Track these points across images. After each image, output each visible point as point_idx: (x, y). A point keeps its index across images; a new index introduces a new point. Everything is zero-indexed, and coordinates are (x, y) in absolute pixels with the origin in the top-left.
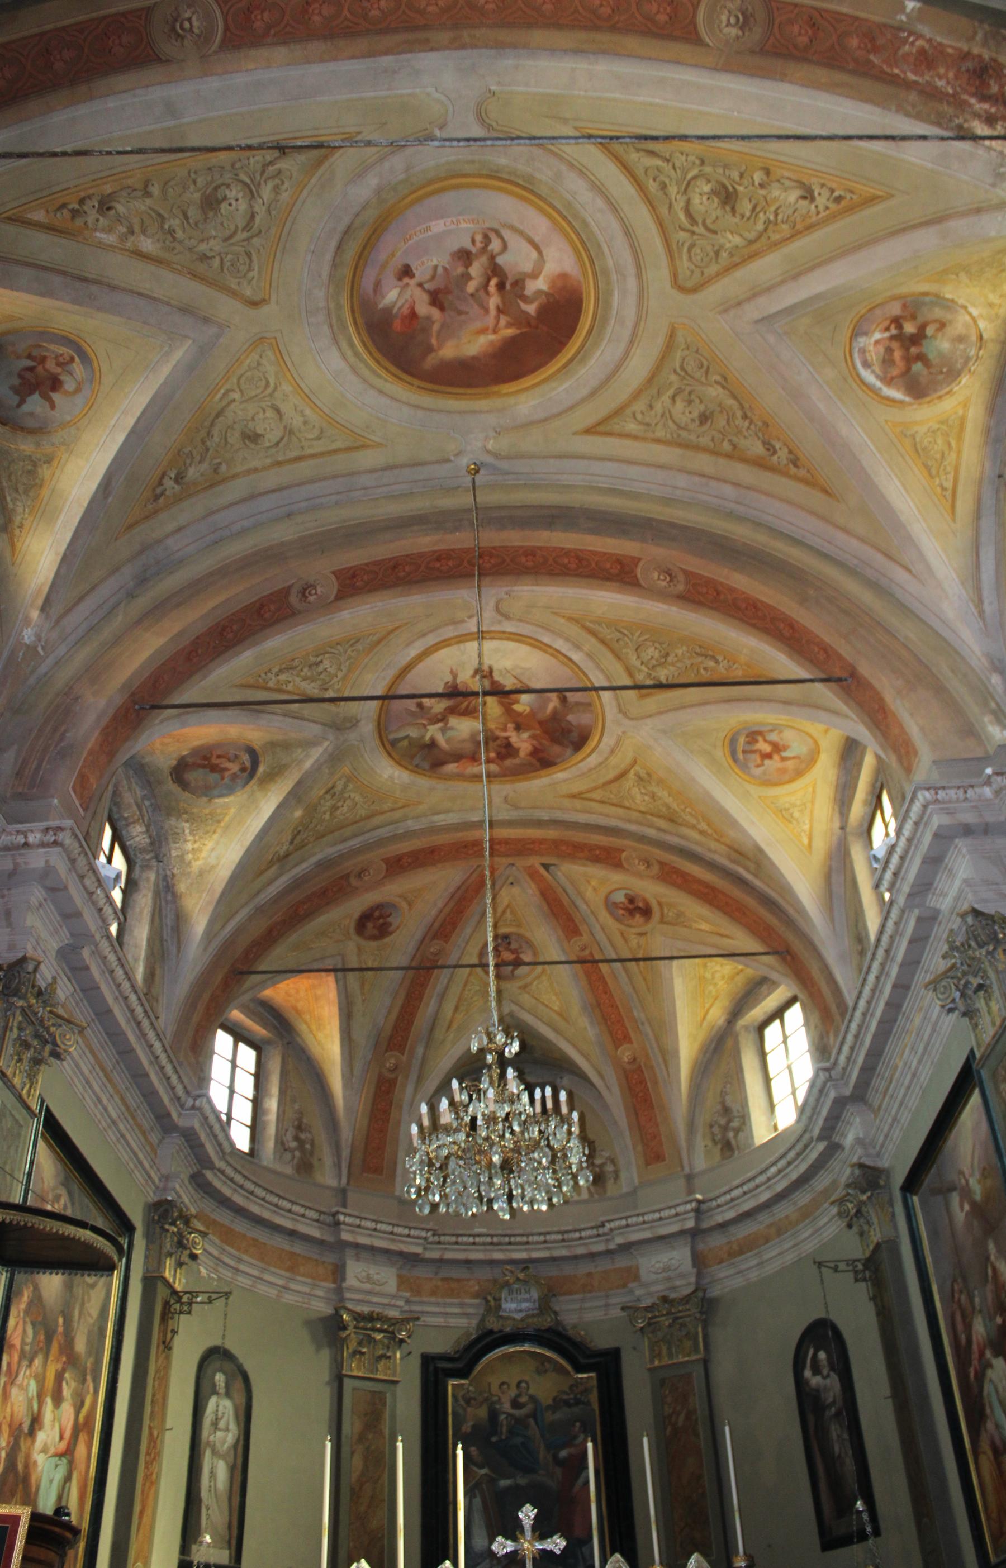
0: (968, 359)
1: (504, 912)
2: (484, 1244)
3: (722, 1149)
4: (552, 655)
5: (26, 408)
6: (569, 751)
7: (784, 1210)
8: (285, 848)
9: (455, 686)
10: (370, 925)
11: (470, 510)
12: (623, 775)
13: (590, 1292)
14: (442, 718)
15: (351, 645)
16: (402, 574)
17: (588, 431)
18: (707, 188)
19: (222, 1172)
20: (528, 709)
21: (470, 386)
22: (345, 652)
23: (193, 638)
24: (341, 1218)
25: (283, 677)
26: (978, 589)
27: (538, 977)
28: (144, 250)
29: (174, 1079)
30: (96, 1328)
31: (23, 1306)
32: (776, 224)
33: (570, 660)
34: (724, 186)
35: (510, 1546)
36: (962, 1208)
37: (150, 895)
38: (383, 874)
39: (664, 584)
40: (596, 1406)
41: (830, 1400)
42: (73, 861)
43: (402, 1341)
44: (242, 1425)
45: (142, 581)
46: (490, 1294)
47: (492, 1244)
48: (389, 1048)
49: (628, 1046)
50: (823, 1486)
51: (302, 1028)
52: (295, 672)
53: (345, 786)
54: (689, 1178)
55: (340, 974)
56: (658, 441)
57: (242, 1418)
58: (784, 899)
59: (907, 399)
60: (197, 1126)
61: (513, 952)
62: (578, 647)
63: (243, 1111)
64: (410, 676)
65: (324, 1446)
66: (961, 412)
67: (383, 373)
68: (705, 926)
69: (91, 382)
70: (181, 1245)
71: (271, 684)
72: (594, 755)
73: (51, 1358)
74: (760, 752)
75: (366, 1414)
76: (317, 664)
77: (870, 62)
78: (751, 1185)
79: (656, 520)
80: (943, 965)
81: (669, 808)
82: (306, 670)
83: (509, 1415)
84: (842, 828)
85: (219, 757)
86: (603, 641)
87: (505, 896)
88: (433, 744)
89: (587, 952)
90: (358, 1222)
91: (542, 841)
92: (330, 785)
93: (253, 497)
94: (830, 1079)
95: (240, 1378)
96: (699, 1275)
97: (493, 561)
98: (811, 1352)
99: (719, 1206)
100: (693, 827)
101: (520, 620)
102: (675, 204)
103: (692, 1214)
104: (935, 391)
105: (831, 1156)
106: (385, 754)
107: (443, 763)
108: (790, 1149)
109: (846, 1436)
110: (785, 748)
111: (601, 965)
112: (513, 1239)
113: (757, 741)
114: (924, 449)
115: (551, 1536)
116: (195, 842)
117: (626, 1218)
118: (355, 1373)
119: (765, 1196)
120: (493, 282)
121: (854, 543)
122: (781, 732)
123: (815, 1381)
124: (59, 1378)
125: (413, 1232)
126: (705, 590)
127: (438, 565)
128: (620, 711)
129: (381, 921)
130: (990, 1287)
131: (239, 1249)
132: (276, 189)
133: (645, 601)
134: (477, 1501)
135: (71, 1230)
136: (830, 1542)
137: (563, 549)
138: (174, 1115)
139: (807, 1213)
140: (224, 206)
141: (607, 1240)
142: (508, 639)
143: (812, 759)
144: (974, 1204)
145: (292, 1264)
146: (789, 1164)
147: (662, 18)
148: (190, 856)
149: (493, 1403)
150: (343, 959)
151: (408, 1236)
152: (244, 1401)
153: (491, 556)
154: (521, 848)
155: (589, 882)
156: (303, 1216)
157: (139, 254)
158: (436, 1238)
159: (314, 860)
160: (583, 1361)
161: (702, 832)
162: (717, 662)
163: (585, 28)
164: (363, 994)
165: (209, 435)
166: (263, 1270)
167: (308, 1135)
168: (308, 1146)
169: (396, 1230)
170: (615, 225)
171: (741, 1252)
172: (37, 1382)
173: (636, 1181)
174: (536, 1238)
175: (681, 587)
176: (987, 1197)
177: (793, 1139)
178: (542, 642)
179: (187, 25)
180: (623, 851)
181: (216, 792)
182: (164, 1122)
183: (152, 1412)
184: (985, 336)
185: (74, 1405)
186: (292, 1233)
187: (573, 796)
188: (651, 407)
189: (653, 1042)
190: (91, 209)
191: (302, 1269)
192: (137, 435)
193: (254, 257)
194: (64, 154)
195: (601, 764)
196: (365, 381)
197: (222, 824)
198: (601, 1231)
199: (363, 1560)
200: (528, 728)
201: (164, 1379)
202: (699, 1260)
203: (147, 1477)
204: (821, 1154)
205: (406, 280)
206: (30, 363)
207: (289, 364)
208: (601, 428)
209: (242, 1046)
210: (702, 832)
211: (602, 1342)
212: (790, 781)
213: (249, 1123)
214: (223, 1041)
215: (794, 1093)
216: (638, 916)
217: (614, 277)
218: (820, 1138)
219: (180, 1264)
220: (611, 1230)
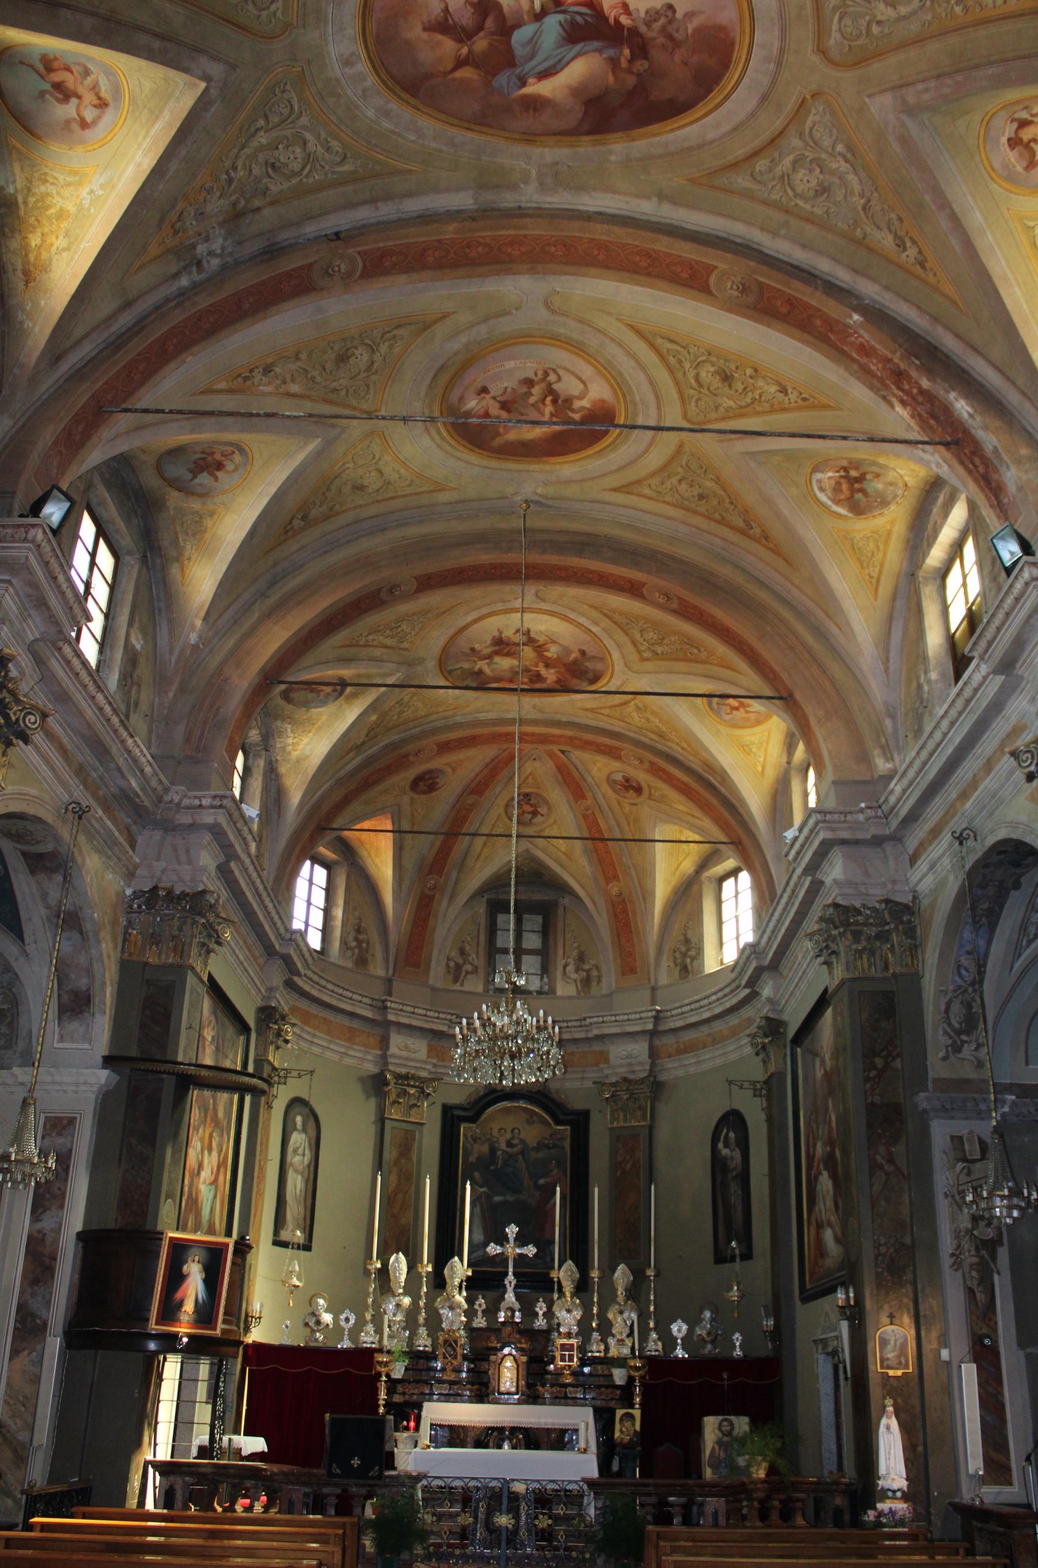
0: (895, 496)
1: (527, 778)
5: (197, 481)
7: (718, 1026)
10: (421, 784)
11: (519, 532)
17: (615, 490)
18: (712, 369)
21: (526, 456)
24: (389, 1004)
25: (370, 637)
26: (887, 651)
28: (292, 392)
32: (760, 401)
34: (724, 371)
35: (499, 1250)
37: (260, 778)
40: (568, 1149)
42: (230, 815)
43: (429, 1094)
45: (272, 584)
48: (430, 872)
50: (721, 1222)
51: (363, 853)
54: (654, 989)
56: (668, 503)
57: (314, 1147)
59: (850, 515)
60: (292, 952)
61: (532, 806)
62: (596, 624)
63: (317, 919)
66: (888, 527)
67: (461, 448)
69: (245, 465)
70: (278, 1034)
71: (361, 643)
75: (400, 1146)
77: (828, 336)
78: (697, 1005)
80: (816, 927)
84: (789, 763)
86: (615, 623)
87: (529, 767)
88: (480, 672)
90: (401, 1007)
93: (356, 522)
94: (755, 952)
96: (653, 1064)
98: (725, 1131)
102: (688, 374)
103: (652, 1020)
104: (871, 511)
108: (727, 986)
114: (859, 549)
119: (707, 1015)
120: (549, 399)
121: (804, 598)
123: (725, 1152)
124: (211, 1137)
125: (441, 1015)
128: (626, 665)
132: (391, 347)
134: (478, 1209)
136: (721, 1258)
138: (277, 947)
139: (734, 1033)
140: (352, 360)
141: (587, 1031)
144: (825, 1071)
145: (350, 1037)
146: (725, 996)
147: (685, 275)
151: (438, 1018)
156: (360, 1002)
157: (289, 395)
159: (381, 744)
160: (562, 1117)
161: (683, 748)
163: (628, 271)
165: (328, 489)
166: (330, 1042)
168: (364, 945)
169: (429, 1013)
170: (642, 377)
171: (685, 1052)
179: (337, 269)
182: (270, 951)
184: (909, 484)
186: (352, 1015)
188: (663, 483)
189: (636, 882)
190: (258, 376)
192: (277, 499)
193: (371, 386)
194: (258, 415)
196: (447, 452)
198: (583, 1023)
200: (554, 667)
202: (654, 1053)
203: (258, 1191)
205: (483, 395)
206: (202, 456)
207: (391, 445)
208: (624, 489)
211: (578, 1105)
212: (752, 726)
213: (320, 927)
215: (737, 938)
216: (631, 791)
217: (640, 406)
219: (278, 1048)
220: (591, 1024)
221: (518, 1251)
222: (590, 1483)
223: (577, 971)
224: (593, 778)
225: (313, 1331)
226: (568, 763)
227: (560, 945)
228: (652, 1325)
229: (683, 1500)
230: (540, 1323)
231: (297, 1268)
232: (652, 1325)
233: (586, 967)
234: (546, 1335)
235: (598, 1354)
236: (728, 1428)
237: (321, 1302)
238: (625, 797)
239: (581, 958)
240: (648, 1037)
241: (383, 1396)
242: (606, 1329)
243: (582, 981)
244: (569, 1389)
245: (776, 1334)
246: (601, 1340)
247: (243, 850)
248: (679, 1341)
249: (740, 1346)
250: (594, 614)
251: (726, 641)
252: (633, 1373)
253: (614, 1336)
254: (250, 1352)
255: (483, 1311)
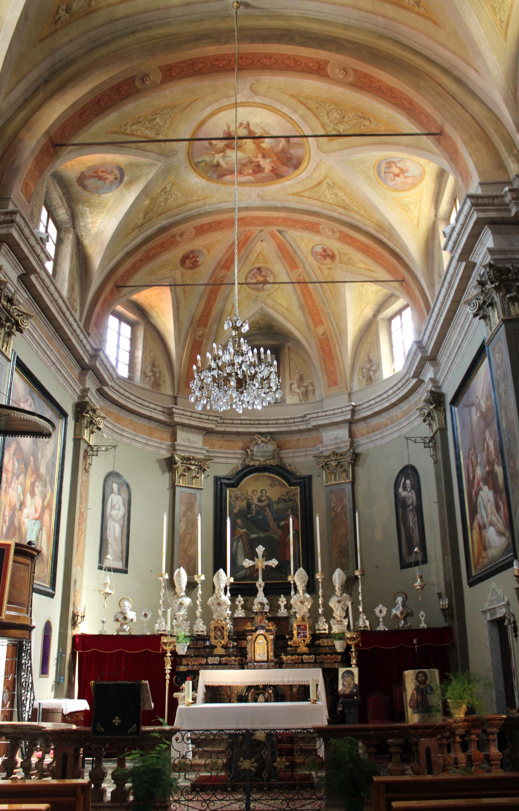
2: (246, 424)
3: (367, 380)
4: (282, 116)
6: (291, 170)
8: (140, 221)
9: (229, 133)
10: (188, 262)
12: (320, 183)
13: (298, 448)
14: (223, 151)
15: (171, 110)
16: (197, 69)
19: (113, 388)
20: (269, 146)
22: (168, 113)
23: (82, 105)
24: (174, 410)
25: (134, 127)
27: (276, 290)
29: (85, 342)
30: (50, 463)
31: (12, 452)
33: (291, 119)
36: (476, 415)
38: (194, 235)
39: (342, 76)
41: (410, 502)
44: (127, 508)
46: (248, 448)
47: (250, 424)
49: (322, 326)
52: (141, 125)
53: (172, 187)
54: (350, 394)
55: (173, 287)
57: (127, 504)
58: (404, 253)
61: (263, 276)
62: (295, 111)
63: (125, 358)
64: (204, 127)
65: (163, 518)
68: (362, 266)
70: (91, 422)
71: (128, 131)
72: (305, 172)
73: (28, 476)
74: (393, 173)
75: (187, 504)
76: (153, 120)
78: (380, 399)
79: (340, 38)
81: (344, 202)
82: (147, 123)
83: (256, 505)
84: (436, 216)
85: (102, 172)
86: (309, 109)
89: (301, 277)
90: (182, 412)
91: (278, 218)
92: (163, 187)
95: (125, 486)
96: (352, 443)
97: (248, 61)
98: (403, 480)
99: (363, 409)
100: (357, 213)
101: (263, 96)
103: (350, 412)
105: (420, 386)
106: (193, 170)
107: (224, 175)
109: (416, 519)
110: (407, 171)
111: (308, 284)
112: (260, 422)
113: (392, 167)
115: (271, 559)
116: (92, 218)
117: (317, 413)
118: (181, 484)
122: (404, 162)
123: (403, 493)
124: (33, 485)
125: (210, 418)
126: (364, 80)
127: (217, 63)
128: (319, 148)
129: (194, 259)
130: (485, 453)
131: (123, 425)
133: (333, 86)
135: (31, 417)
136: (404, 565)
137: (286, 55)
141: (307, 424)
142: (257, 107)
143: (421, 178)
144: (481, 412)
146: (399, 389)
148: (90, 225)
149: (249, 500)
150: (174, 280)
151: (208, 419)
152: (127, 497)
153: (247, 58)
154: (267, 222)
155: (302, 240)
156: (155, 409)
158: (222, 421)
161: (361, 216)
162: (370, 122)
164: (185, 298)
167: (158, 369)
168: (158, 375)
171: (373, 431)
172: (22, 487)
173: (323, 395)
174: (272, 422)
175: (351, 79)
176: (488, 409)
177: (402, 375)
178: (276, 109)
180: (320, 224)
181: (102, 191)
183: (81, 501)
185: (42, 498)
186: (150, 418)
187: (294, 194)
191: (155, 435)
195: (308, 177)
197: (106, 208)
198: (304, 419)
199: (182, 568)
201: (86, 485)
202: (351, 434)
204: (414, 385)
209: (123, 324)
210: (361, 216)
211: (304, 472)
212: (409, 189)
213: (128, 363)
214: (112, 321)
216: (328, 259)
218: (413, 377)
220: (310, 419)
221: (266, 563)
222: (320, 731)
223: (299, 387)
224: (302, 252)
225: (122, 625)
226: (285, 241)
227: (287, 371)
228: (361, 610)
229: (400, 741)
230: (283, 612)
231: (109, 581)
232: (361, 610)
233: (305, 384)
234: (287, 619)
235: (323, 632)
236: (423, 678)
237: (127, 603)
238: (324, 264)
239: (301, 379)
240: (348, 424)
241: (168, 667)
242: (329, 614)
243: (302, 394)
244: (305, 657)
245: (447, 612)
246: (326, 622)
247: (39, 265)
248: (381, 620)
249: (424, 620)
250: (293, 102)
251: (390, 102)
252: (350, 642)
253: (334, 618)
254: (77, 640)
255: (242, 606)
